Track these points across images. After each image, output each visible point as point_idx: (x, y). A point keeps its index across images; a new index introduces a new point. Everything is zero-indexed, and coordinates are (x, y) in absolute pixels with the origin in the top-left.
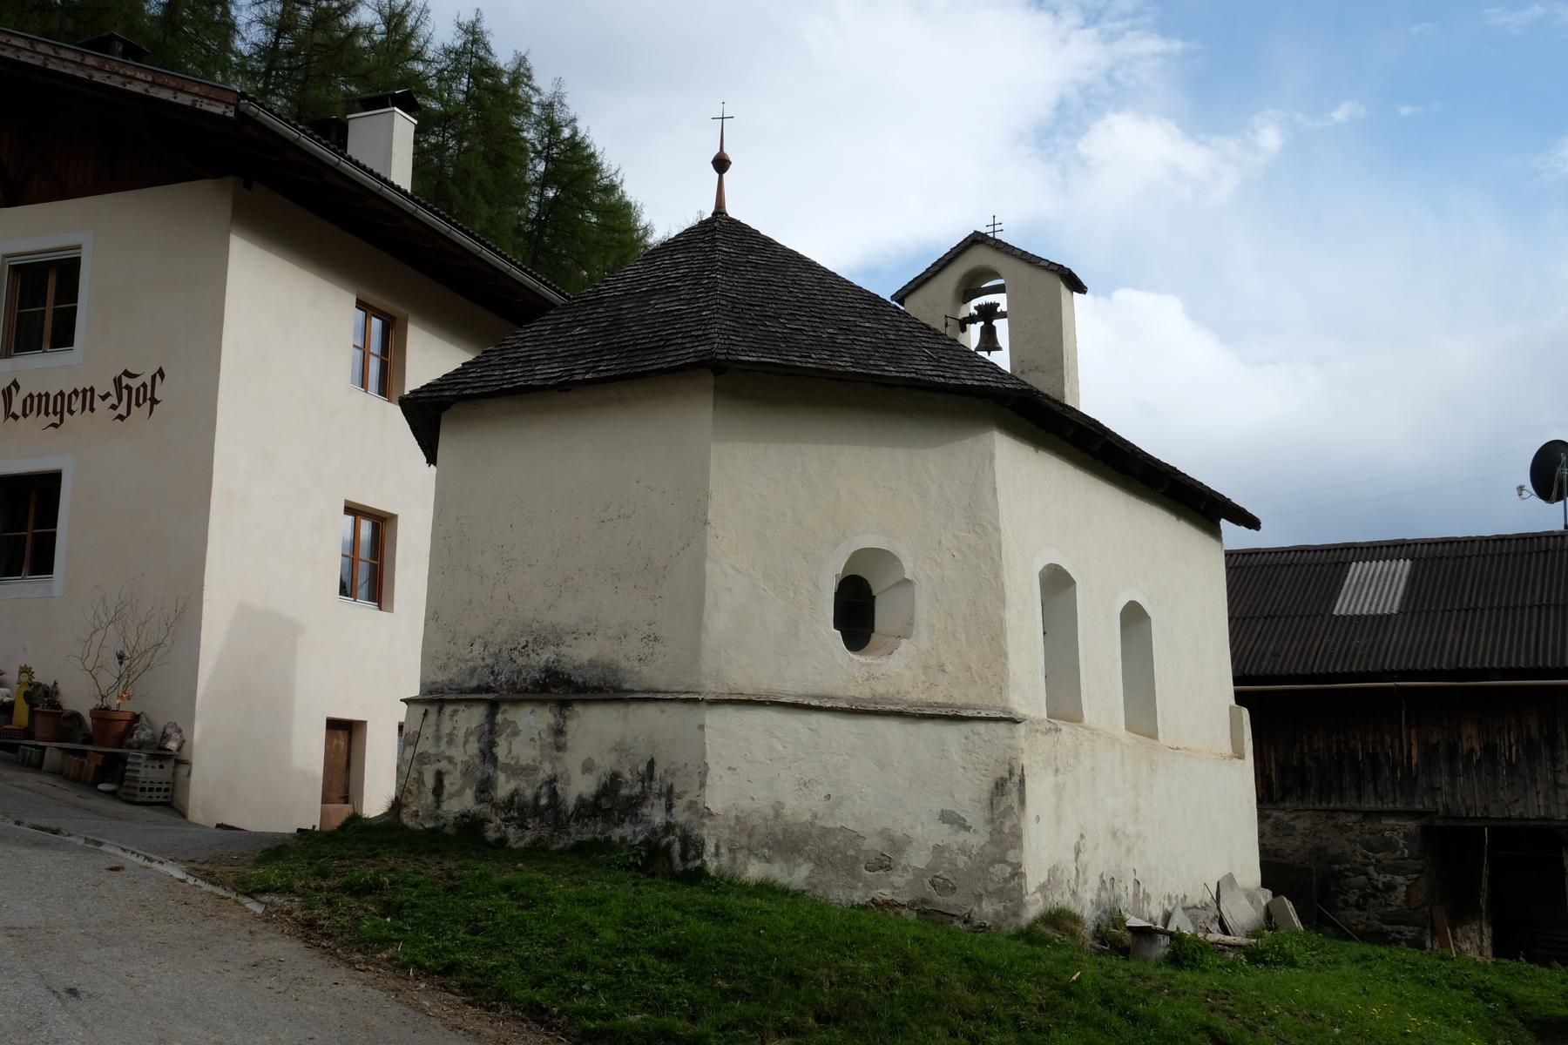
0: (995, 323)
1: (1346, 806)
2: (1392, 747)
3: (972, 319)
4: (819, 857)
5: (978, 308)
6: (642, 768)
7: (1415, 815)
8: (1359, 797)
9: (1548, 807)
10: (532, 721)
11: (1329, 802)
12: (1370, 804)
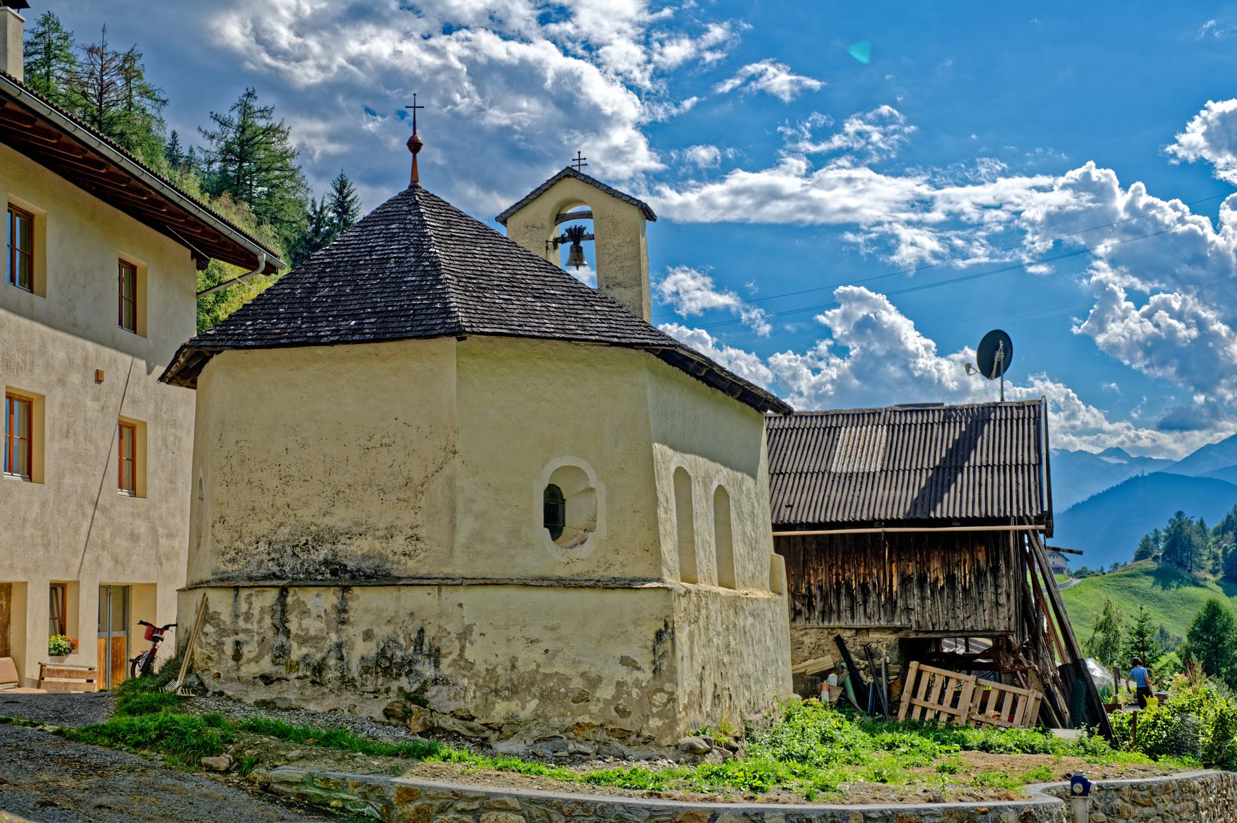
0: (582, 244)
1: (843, 624)
2: (878, 578)
3: (563, 240)
4: (542, 695)
5: (569, 231)
6: (414, 636)
7: (896, 630)
8: (853, 617)
9: (991, 622)
10: (322, 601)
11: (830, 621)
12: (861, 622)
